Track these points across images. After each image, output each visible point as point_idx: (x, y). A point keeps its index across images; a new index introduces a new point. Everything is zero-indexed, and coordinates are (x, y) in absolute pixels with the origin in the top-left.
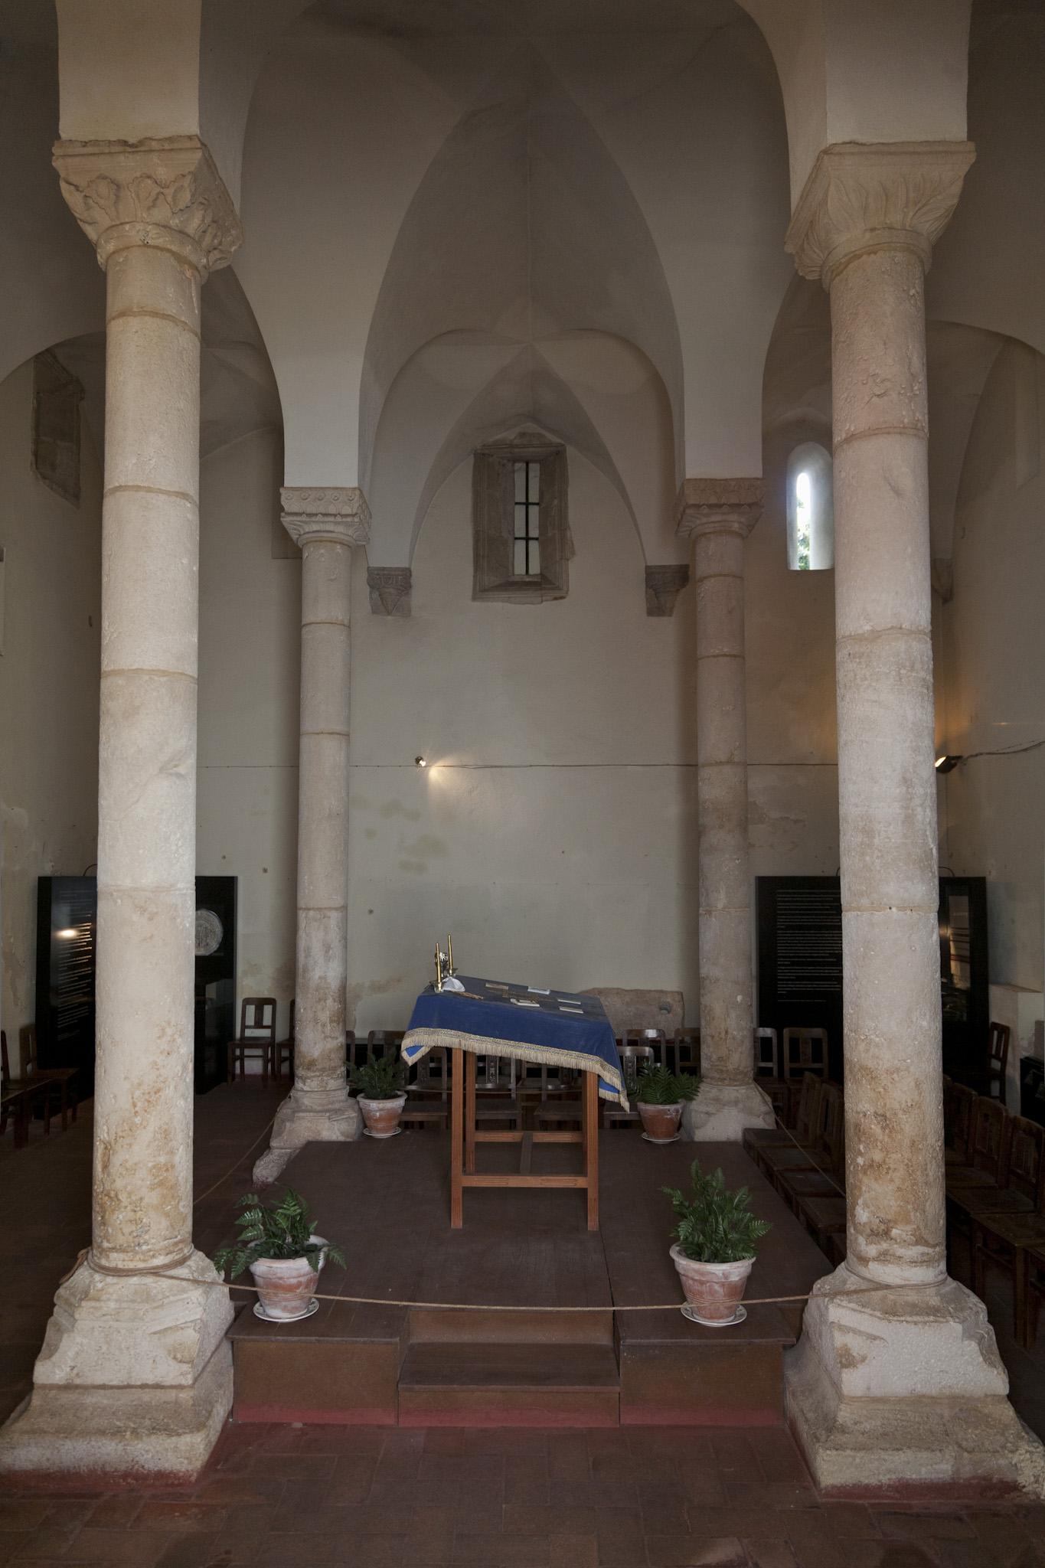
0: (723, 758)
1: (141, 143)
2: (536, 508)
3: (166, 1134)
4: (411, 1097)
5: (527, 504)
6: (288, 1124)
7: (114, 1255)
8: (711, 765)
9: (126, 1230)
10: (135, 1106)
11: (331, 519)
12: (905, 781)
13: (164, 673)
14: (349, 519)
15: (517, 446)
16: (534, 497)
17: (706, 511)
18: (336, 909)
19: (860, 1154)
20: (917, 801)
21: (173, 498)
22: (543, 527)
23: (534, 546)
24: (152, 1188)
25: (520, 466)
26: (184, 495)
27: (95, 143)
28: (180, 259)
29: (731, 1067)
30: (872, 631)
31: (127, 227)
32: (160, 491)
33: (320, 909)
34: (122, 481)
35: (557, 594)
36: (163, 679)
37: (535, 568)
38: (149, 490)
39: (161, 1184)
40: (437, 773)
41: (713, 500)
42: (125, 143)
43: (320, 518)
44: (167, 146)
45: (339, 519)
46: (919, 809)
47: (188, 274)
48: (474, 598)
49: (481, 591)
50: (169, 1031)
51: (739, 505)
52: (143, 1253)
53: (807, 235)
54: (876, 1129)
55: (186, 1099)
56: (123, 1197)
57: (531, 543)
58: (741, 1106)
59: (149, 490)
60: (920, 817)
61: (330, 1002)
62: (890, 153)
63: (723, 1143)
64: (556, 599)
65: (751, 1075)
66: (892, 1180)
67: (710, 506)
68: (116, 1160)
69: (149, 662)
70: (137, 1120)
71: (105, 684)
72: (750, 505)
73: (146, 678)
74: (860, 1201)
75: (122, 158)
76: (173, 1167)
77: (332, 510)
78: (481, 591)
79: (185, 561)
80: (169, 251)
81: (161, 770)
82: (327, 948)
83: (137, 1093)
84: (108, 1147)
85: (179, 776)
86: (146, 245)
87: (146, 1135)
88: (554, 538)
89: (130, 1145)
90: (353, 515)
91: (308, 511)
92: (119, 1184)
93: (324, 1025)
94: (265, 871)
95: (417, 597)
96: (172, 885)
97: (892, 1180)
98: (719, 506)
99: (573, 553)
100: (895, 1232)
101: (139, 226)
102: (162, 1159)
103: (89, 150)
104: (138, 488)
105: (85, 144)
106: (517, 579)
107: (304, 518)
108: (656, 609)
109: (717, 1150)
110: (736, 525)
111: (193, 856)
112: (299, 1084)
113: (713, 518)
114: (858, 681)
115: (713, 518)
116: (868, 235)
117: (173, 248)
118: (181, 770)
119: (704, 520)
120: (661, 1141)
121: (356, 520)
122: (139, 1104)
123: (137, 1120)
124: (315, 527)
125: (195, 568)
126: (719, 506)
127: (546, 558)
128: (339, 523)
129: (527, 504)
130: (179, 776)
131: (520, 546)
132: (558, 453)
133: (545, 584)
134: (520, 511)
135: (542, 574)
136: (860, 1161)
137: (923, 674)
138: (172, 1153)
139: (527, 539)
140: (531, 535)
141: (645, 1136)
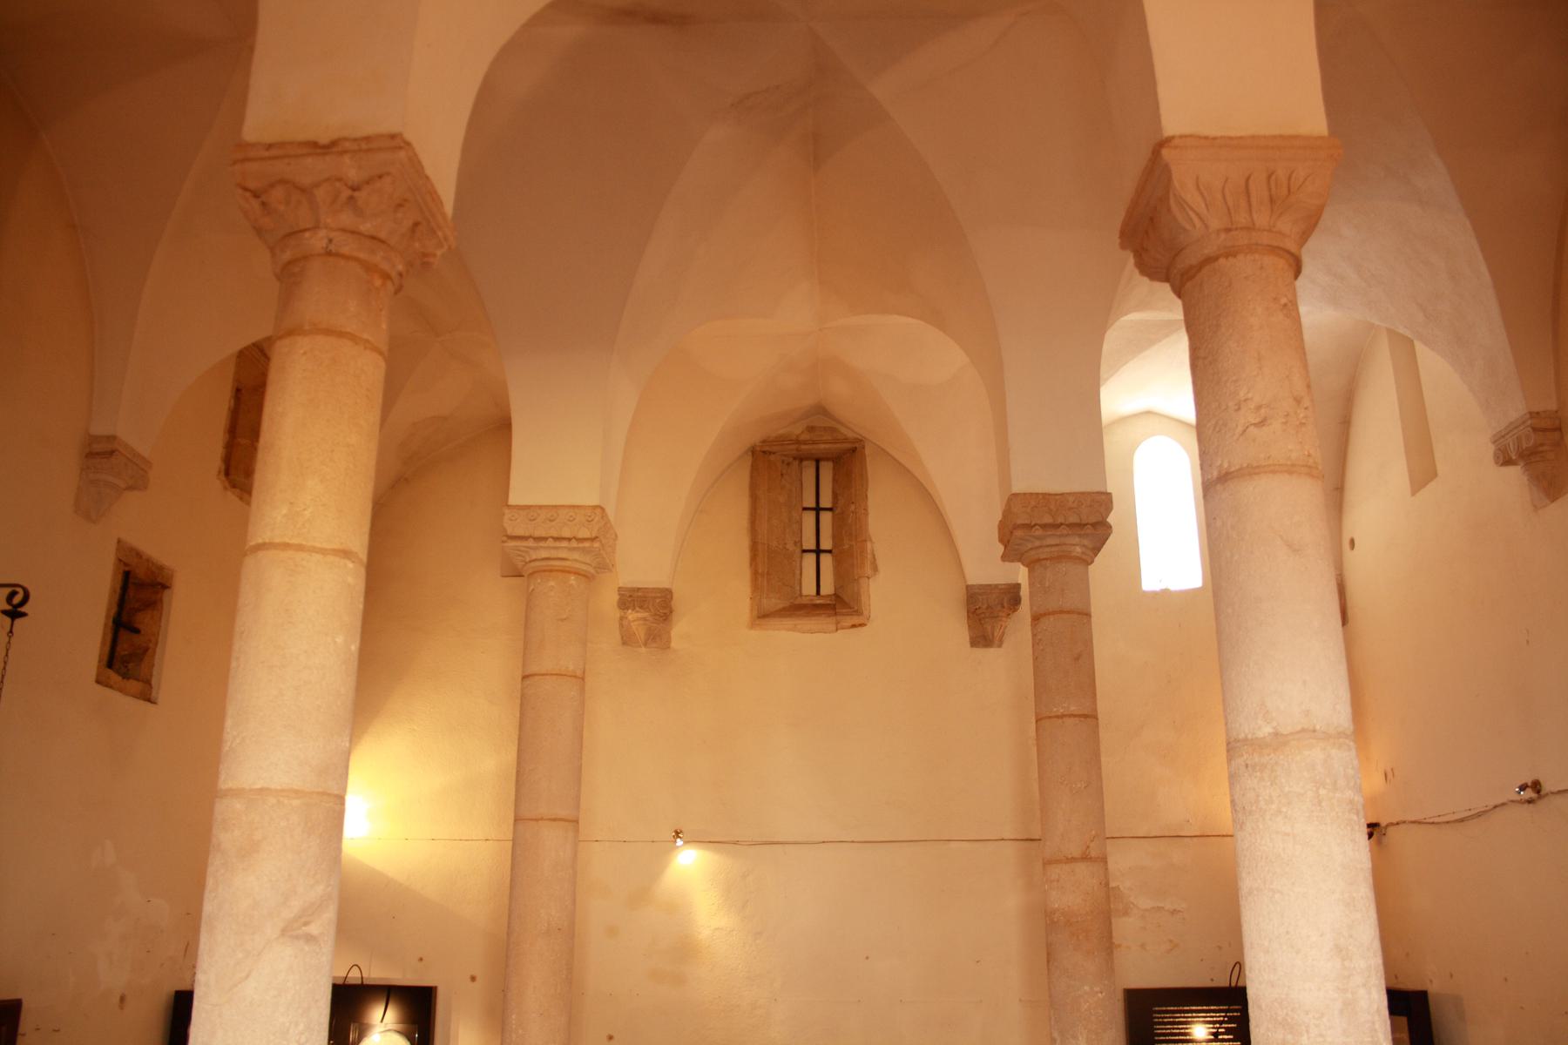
0: (1076, 853)
1: (334, 143)
5: (818, 510)
11: (564, 544)
12: (1340, 951)
13: (297, 793)
14: (587, 544)
15: (805, 443)
17: (1038, 532)
21: (331, 558)
22: (837, 537)
23: (826, 560)
26: (346, 554)
27: (282, 145)
28: (369, 268)
30: (1276, 734)
31: (307, 235)
32: (314, 550)
35: (856, 620)
36: (296, 802)
37: (828, 588)
40: (689, 864)
41: (1048, 519)
42: (315, 145)
43: (550, 543)
44: (364, 146)
45: (574, 544)
46: (1362, 992)
47: (378, 282)
48: (752, 626)
49: (762, 616)
51: (1081, 525)
57: (823, 557)
64: (854, 626)
67: (1044, 526)
71: (221, 807)
72: (1094, 525)
75: (309, 160)
77: (567, 534)
78: (762, 616)
79: (340, 639)
80: (357, 259)
81: (284, 932)
85: (310, 938)
86: (329, 254)
88: (848, 551)
90: (593, 540)
91: (537, 534)
94: (473, 979)
95: (680, 629)
98: (1057, 526)
99: (875, 569)
101: (322, 233)
103: (274, 152)
105: (270, 146)
106: (805, 601)
107: (531, 543)
108: (982, 637)
110: (1078, 549)
113: (1050, 541)
114: (1262, 803)
115: (1050, 541)
116: (1223, 236)
117: (362, 255)
118: (314, 929)
119: (1037, 543)
121: (596, 545)
124: (544, 554)
125: (354, 647)
126: (1057, 526)
127: (841, 575)
128: (574, 549)
129: (818, 510)
130: (310, 938)
131: (810, 560)
132: (854, 450)
133: (840, 605)
134: (809, 519)
135: (836, 595)
139: (818, 552)
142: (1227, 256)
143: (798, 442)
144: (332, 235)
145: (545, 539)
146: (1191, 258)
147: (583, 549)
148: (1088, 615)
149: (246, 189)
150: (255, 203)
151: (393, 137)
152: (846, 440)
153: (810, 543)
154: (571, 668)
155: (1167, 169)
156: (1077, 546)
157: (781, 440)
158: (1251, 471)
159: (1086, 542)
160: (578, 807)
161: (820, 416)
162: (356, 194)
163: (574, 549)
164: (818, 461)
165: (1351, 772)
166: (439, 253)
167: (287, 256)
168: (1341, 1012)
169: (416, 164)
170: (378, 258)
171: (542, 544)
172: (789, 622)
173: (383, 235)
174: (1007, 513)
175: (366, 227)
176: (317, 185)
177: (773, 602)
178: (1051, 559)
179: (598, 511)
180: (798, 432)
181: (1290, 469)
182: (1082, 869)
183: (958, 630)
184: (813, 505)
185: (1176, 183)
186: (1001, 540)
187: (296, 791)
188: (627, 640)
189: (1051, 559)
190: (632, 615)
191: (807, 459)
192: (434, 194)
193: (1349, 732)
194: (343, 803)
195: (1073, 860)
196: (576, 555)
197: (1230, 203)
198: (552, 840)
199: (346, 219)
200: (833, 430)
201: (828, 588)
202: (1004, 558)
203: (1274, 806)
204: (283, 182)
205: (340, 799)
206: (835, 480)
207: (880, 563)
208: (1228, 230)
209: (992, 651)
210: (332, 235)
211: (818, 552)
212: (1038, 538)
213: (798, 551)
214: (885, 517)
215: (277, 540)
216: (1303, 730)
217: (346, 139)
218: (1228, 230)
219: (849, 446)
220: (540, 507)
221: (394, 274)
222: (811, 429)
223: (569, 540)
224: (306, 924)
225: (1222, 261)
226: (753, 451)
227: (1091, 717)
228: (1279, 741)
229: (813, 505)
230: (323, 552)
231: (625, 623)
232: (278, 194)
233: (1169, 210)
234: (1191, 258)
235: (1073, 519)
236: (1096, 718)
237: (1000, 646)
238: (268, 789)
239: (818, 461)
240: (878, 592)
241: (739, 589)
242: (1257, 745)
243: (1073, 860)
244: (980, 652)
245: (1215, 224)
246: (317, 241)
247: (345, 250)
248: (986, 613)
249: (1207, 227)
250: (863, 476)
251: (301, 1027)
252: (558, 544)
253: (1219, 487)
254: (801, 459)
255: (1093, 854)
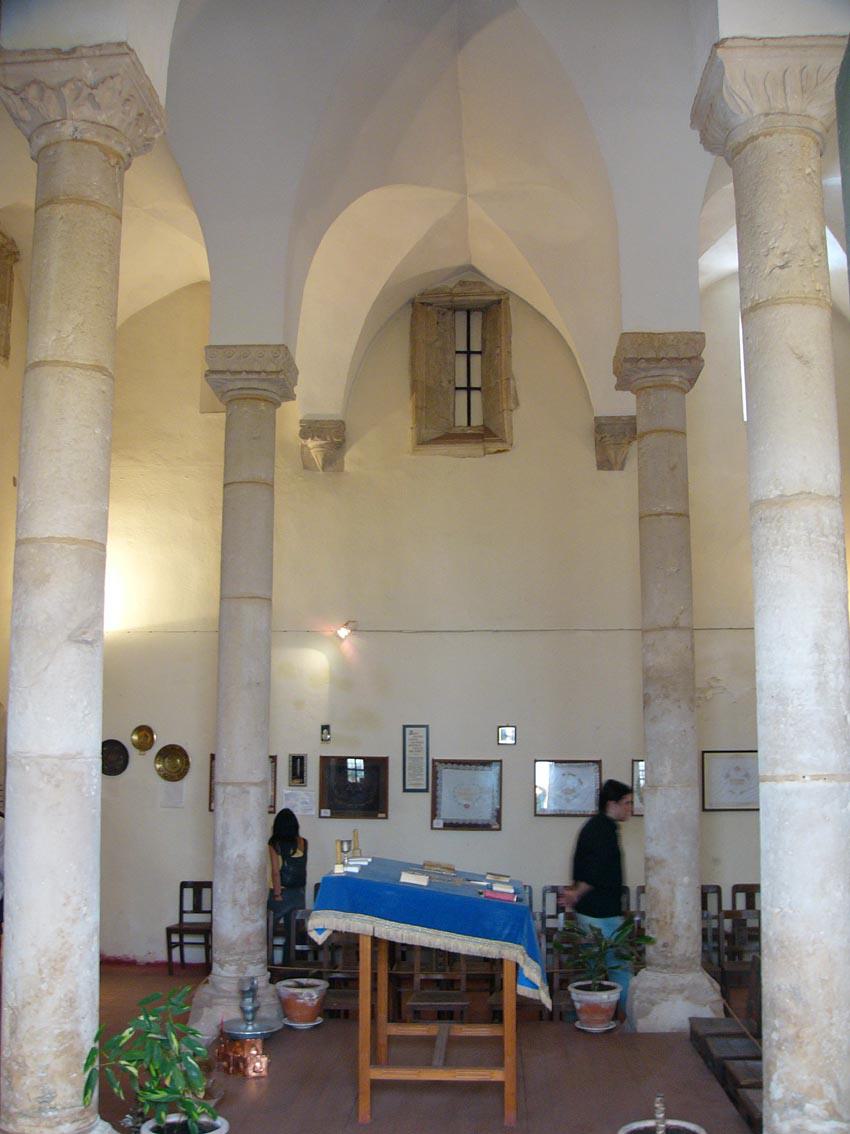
1: (74, 50)
2: (478, 357)
3: (72, 1001)
4: (333, 983)
5: (469, 353)
6: (206, 1010)
7: (22, 1121)
8: (655, 630)
9: (33, 1095)
10: (40, 971)
11: (255, 376)
12: (818, 647)
13: (74, 541)
15: (458, 295)
16: (476, 346)
17: (643, 364)
18: (255, 784)
19: (774, 1029)
20: (829, 668)
24: (57, 1055)
25: (461, 318)
27: (32, 52)
29: (676, 953)
30: (781, 496)
31: (58, 125)
33: (239, 784)
34: (41, 356)
35: (500, 446)
36: (73, 547)
37: (477, 420)
38: (67, 364)
39: (65, 1051)
41: (651, 354)
45: (263, 375)
46: (832, 676)
49: (421, 442)
50: (75, 900)
52: (49, 1118)
53: (708, 116)
54: (789, 1003)
55: (91, 969)
56: (29, 1062)
58: (686, 993)
59: (67, 364)
60: (832, 684)
61: (249, 883)
62: (777, 47)
63: (669, 1033)
64: (499, 451)
65: (699, 961)
66: (805, 1055)
67: (648, 360)
68: (24, 1026)
69: (60, 530)
70: (44, 987)
72: (689, 359)
73: (57, 545)
74: (775, 1077)
75: (56, 64)
76: (78, 1035)
78: (421, 442)
82: (247, 825)
83: (43, 960)
84: (15, 1019)
86: (75, 140)
87: (50, 1003)
88: (495, 389)
89: (37, 1012)
92: (27, 1049)
93: (243, 908)
95: (351, 455)
96: (79, 754)
97: (805, 1055)
100: (808, 1106)
101: (69, 122)
102: (68, 1027)
104: (56, 363)
107: (228, 376)
109: (661, 1041)
110: (677, 379)
111: (100, 724)
112: (216, 968)
113: (653, 372)
115: (653, 372)
117: (100, 140)
120: (595, 1029)
122: (46, 971)
123: (44, 987)
124: (240, 385)
127: (489, 410)
128: (264, 380)
129: (469, 353)
133: (488, 435)
134: (461, 361)
136: (775, 1036)
137: (833, 539)
138: (77, 1021)
139: (469, 389)
140: (473, 385)
141: (578, 1024)
142: (765, 135)
143: (451, 294)
144: (77, 124)
145: (241, 372)
146: (740, 137)
147: (269, 380)
148: (683, 433)
149: (6, 88)
150: (16, 99)
151: (120, 44)
152: (493, 292)
153: (462, 382)
154: (263, 477)
155: (721, 66)
156: (675, 376)
157: (437, 292)
158: (774, 302)
159: (683, 374)
160: (271, 588)
161: (469, 274)
162: (94, 92)
163: (264, 380)
164: (469, 313)
165: (835, 524)
166: (156, 136)
167: (42, 141)
168: (817, 689)
169: (137, 65)
170: (111, 143)
171: (238, 376)
172: (443, 448)
173: (115, 124)
174: (620, 349)
175: (102, 118)
176: (64, 84)
177: (432, 433)
178: (654, 386)
179: (282, 349)
180: (451, 285)
181: (804, 301)
182: (672, 635)
183: (589, 457)
184: (465, 349)
185: (727, 75)
186: (615, 373)
187: (74, 540)
188: (307, 465)
189: (654, 386)
190: (310, 443)
191: (461, 310)
192: (151, 89)
193: (836, 495)
194: (105, 551)
195: (665, 628)
196: (265, 385)
197: (770, 93)
198: (250, 613)
199: (87, 111)
200: (482, 284)
201: (477, 420)
202: (619, 387)
203: (778, 547)
204: (35, 82)
205: (103, 547)
206: (484, 328)
207: (521, 397)
208: (767, 115)
209: (616, 473)
210: (77, 124)
211: (469, 389)
212: (644, 370)
213: (453, 388)
214: (526, 359)
215: (49, 359)
216: (801, 493)
217: (82, 46)
218: (767, 115)
219: (495, 298)
220: (235, 346)
221: (124, 155)
222: (462, 283)
223: (259, 373)
224: (84, 633)
225: (761, 139)
226: (413, 302)
227: (684, 515)
228: (783, 501)
229: (465, 349)
230: (82, 367)
231: (305, 450)
232: (33, 92)
233: (723, 99)
234: (740, 137)
235: (672, 354)
236: (688, 517)
237: (622, 469)
238: (53, 538)
239: (469, 313)
240: (522, 421)
241: (402, 420)
242: (770, 503)
243: (665, 628)
244: (605, 474)
245: (757, 110)
246: (67, 130)
247: (87, 136)
248: (611, 440)
249: (751, 111)
250: (509, 330)
251: (85, 703)
252: (250, 376)
253: (752, 314)
254: (454, 309)
255: (682, 623)
